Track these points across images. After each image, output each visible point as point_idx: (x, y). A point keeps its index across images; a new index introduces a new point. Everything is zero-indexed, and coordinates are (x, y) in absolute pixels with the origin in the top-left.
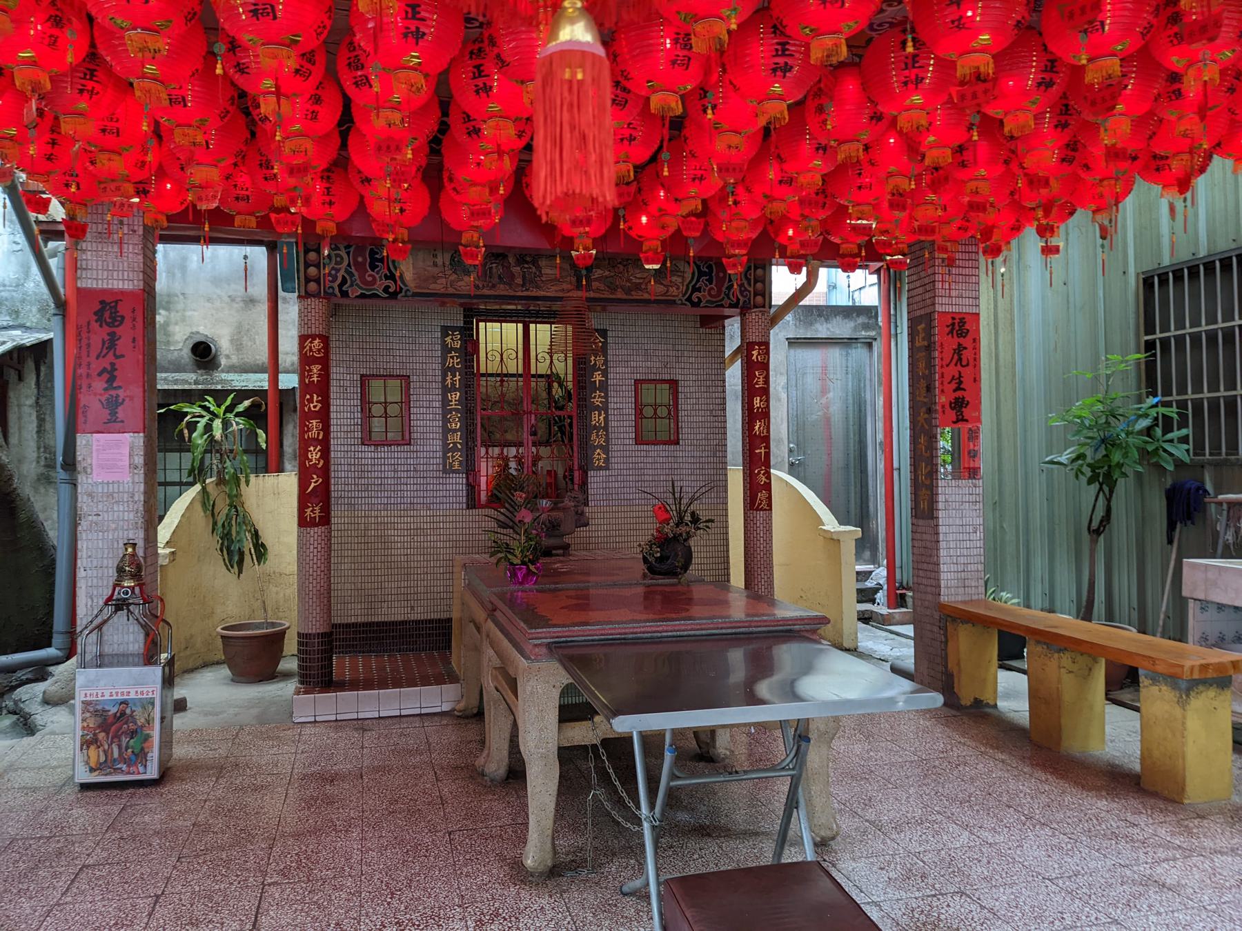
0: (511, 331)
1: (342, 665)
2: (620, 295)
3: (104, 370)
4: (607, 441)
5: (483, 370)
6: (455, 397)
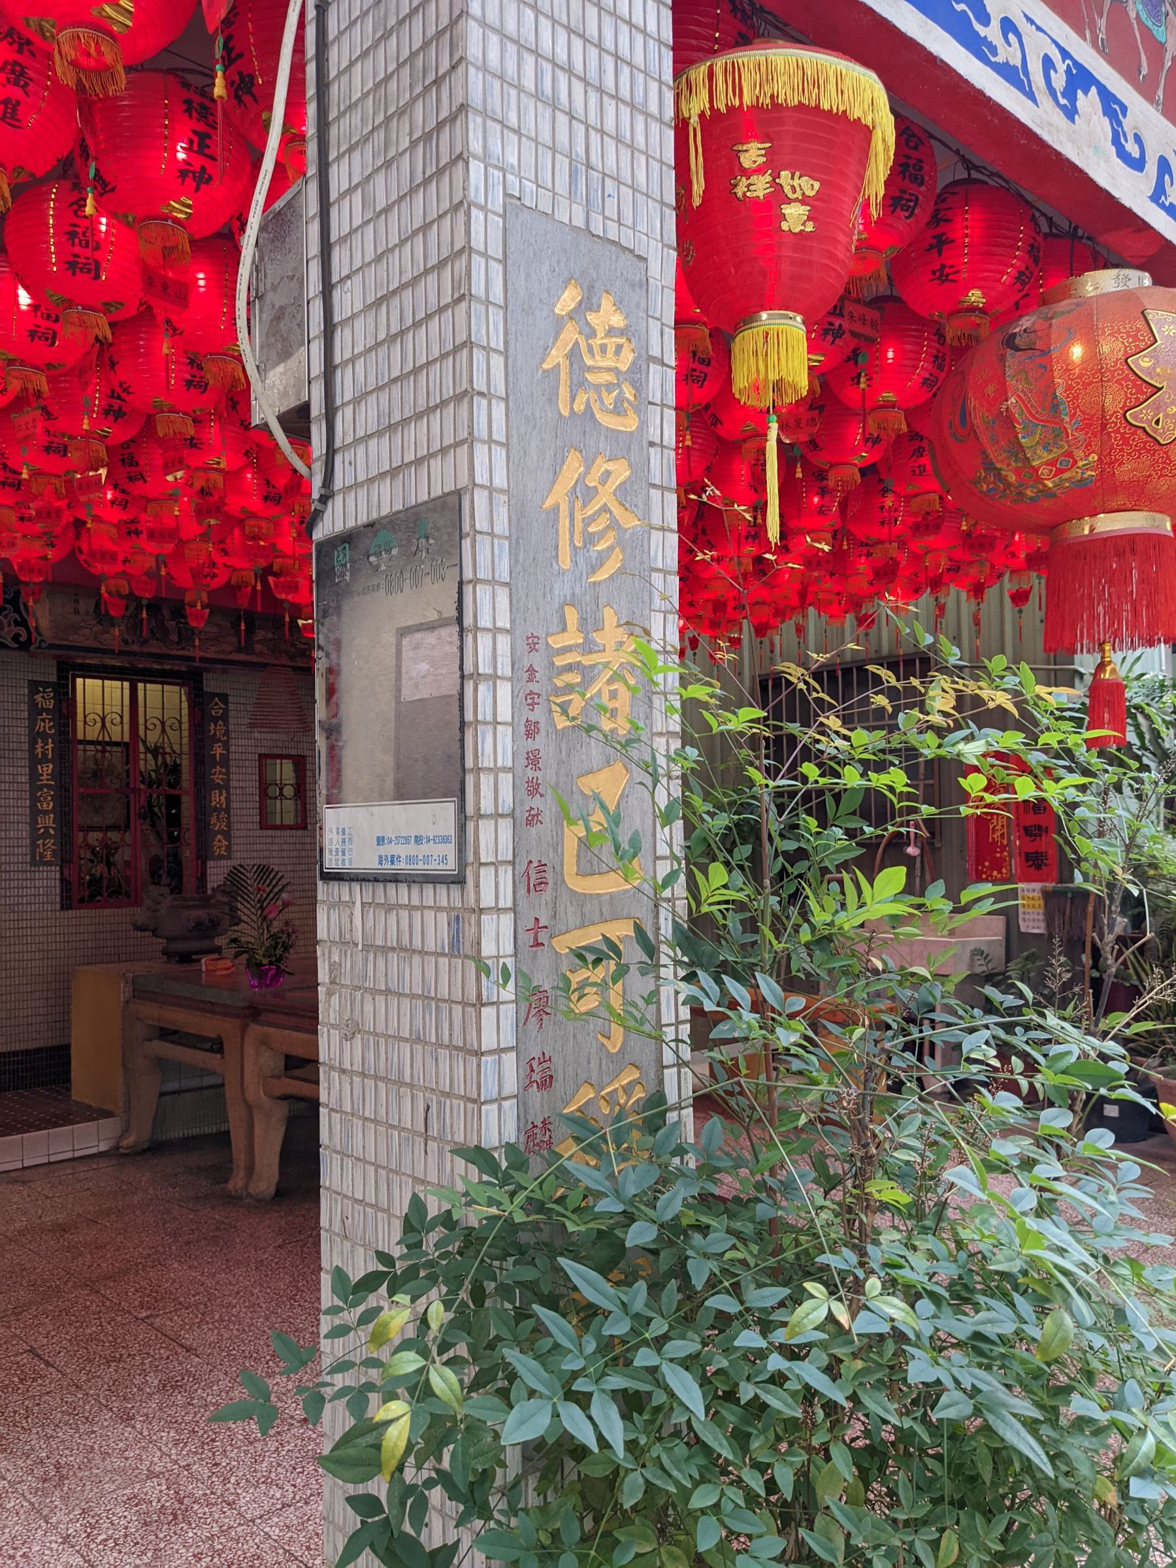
0: (115, 690)
5: (80, 736)
6: (46, 770)
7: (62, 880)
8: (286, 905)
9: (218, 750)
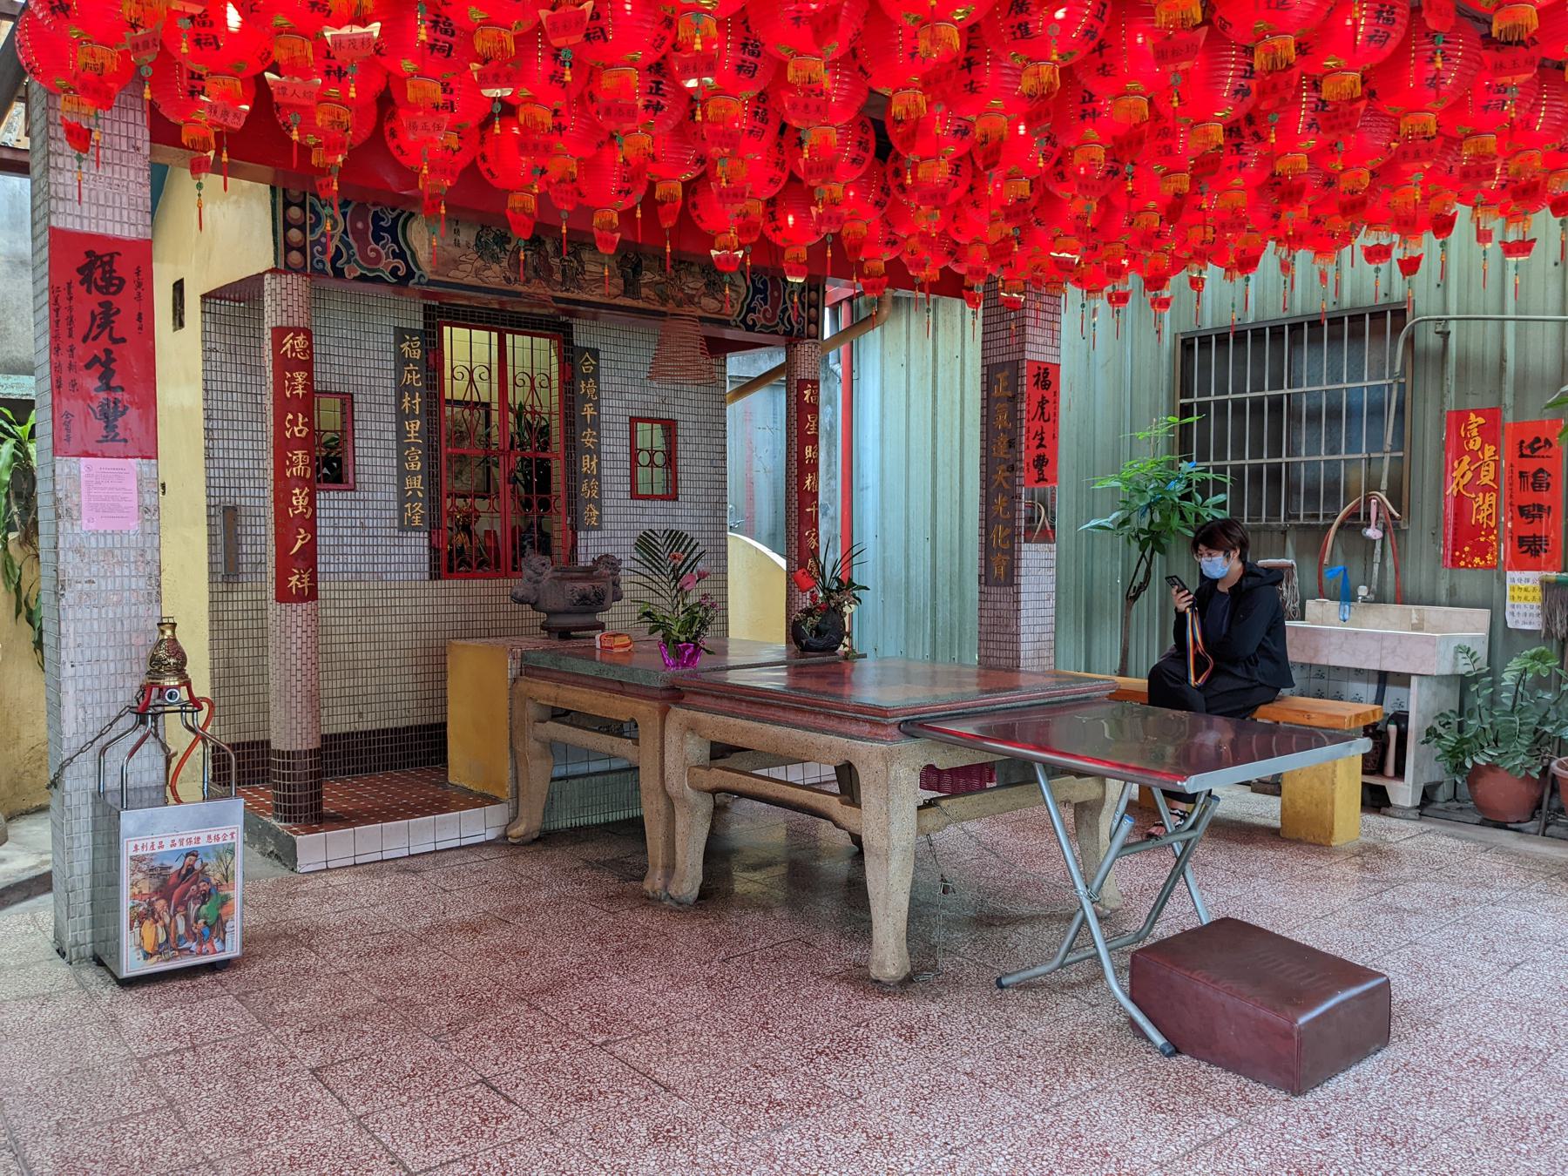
0: (483, 341)
1: (334, 796)
2: (670, 307)
3: (95, 359)
4: (600, 493)
5: (448, 396)
6: (414, 427)
7: (431, 547)
8: (702, 576)
9: (589, 411)
